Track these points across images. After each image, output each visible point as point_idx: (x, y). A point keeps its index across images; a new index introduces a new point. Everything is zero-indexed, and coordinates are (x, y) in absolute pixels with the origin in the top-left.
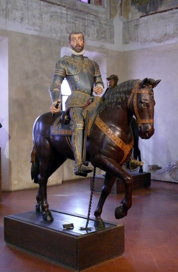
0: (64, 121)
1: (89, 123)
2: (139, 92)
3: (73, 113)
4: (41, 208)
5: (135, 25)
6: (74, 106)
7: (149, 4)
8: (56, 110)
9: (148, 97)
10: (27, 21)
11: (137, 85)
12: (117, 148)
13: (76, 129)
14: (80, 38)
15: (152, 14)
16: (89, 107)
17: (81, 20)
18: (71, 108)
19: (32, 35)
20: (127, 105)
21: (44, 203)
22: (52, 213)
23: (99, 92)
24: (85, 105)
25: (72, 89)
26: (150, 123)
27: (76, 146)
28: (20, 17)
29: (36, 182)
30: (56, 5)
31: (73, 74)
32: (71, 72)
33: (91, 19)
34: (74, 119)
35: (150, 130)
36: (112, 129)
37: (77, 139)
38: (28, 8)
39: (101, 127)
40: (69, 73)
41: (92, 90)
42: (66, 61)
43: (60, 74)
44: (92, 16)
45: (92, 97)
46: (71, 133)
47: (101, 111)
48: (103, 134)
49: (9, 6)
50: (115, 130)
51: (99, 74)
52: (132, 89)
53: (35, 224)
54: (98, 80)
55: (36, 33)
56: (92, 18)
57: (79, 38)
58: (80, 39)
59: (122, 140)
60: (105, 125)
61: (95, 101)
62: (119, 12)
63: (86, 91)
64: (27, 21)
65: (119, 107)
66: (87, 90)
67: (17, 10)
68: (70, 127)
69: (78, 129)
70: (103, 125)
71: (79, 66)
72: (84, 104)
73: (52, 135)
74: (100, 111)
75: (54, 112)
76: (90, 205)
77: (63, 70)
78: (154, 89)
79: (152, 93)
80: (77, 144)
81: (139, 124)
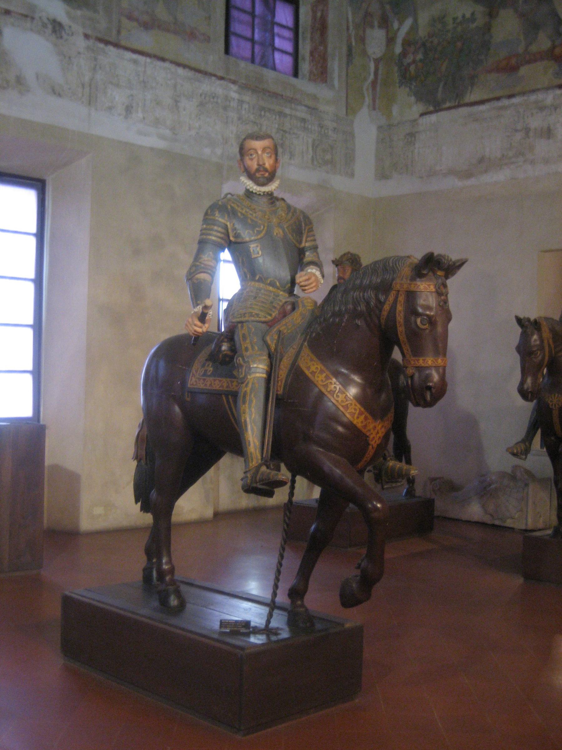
0: (221, 356)
1: (282, 363)
2: (413, 288)
3: (243, 337)
4: (155, 574)
5: (407, 134)
6: (246, 319)
7: (441, 85)
8: (201, 327)
9: (432, 301)
10: (140, 115)
11: (406, 271)
12: (350, 426)
13: (249, 377)
14: (268, 150)
15: (449, 108)
16: (284, 322)
17: (274, 117)
18: (240, 325)
19: (152, 149)
20: (379, 321)
21: (164, 561)
22: (184, 588)
23: (309, 285)
24: (275, 318)
25: (244, 278)
26: (437, 368)
27: (248, 420)
28: (123, 104)
29: (145, 508)
30: (213, 78)
31: (247, 239)
32: (242, 234)
33: (299, 114)
34: (244, 353)
35: (435, 384)
36: (340, 380)
37: (251, 402)
38: (144, 82)
39: (313, 373)
40: (237, 236)
41: (293, 282)
42: (231, 206)
43: (214, 238)
44: (303, 108)
45: (291, 299)
46: (236, 386)
47: (314, 335)
48: (316, 390)
49: (99, 76)
50: (346, 382)
51: (313, 243)
52: (393, 279)
53: (137, 614)
54: (309, 256)
55: (161, 144)
56: (301, 112)
57: (264, 150)
58: (268, 153)
59: (365, 408)
60: (323, 367)
61: (300, 308)
62: (368, 100)
63: (278, 284)
64: (140, 115)
65: (359, 323)
66: (279, 280)
67: (118, 85)
68: (235, 373)
69: (253, 376)
70: (317, 368)
71: (260, 219)
72: (271, 315)
73: (189, 392)
74: (312, 332)
75: (195, 331)
76: (279, 572)
77: (222, 228)
78: (449, 282)
79: (444, 291)
80: (251, 415)
81: (408, 369)
